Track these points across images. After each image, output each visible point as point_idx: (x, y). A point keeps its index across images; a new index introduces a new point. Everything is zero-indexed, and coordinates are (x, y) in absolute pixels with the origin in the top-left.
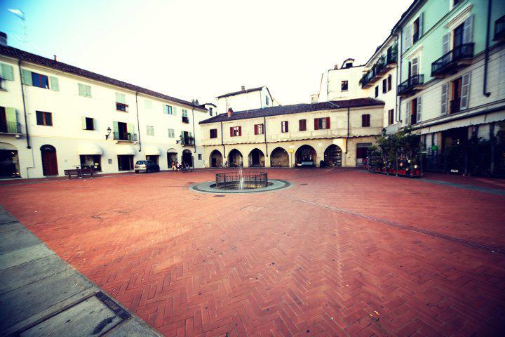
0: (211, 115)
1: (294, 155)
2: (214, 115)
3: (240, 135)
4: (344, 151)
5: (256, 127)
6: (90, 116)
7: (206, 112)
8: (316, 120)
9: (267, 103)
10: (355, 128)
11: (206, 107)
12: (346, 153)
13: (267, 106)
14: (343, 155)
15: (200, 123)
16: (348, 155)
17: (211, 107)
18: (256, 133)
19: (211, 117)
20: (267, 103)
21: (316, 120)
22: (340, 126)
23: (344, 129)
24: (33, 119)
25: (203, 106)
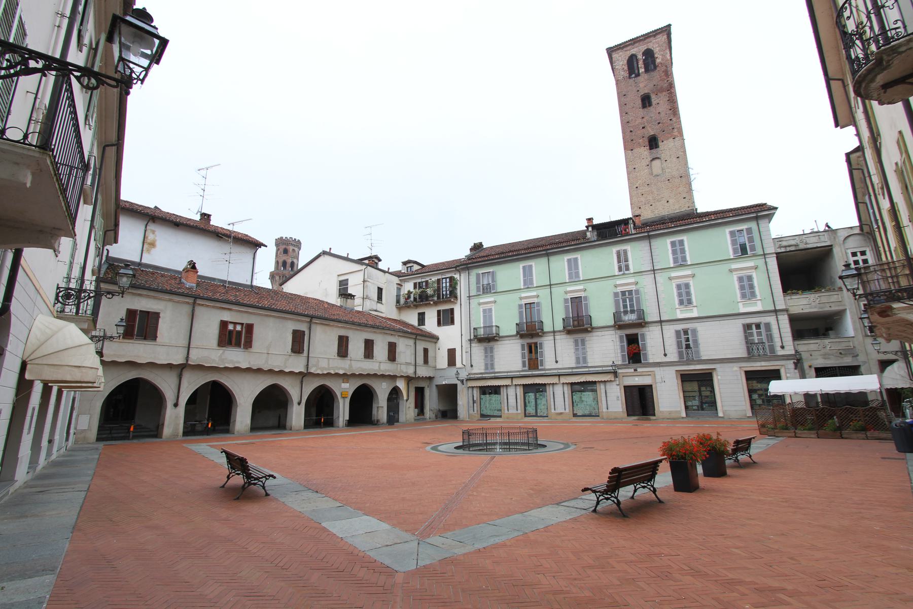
1: (348, 401)
10: (400, 367)
12: (407, 400)
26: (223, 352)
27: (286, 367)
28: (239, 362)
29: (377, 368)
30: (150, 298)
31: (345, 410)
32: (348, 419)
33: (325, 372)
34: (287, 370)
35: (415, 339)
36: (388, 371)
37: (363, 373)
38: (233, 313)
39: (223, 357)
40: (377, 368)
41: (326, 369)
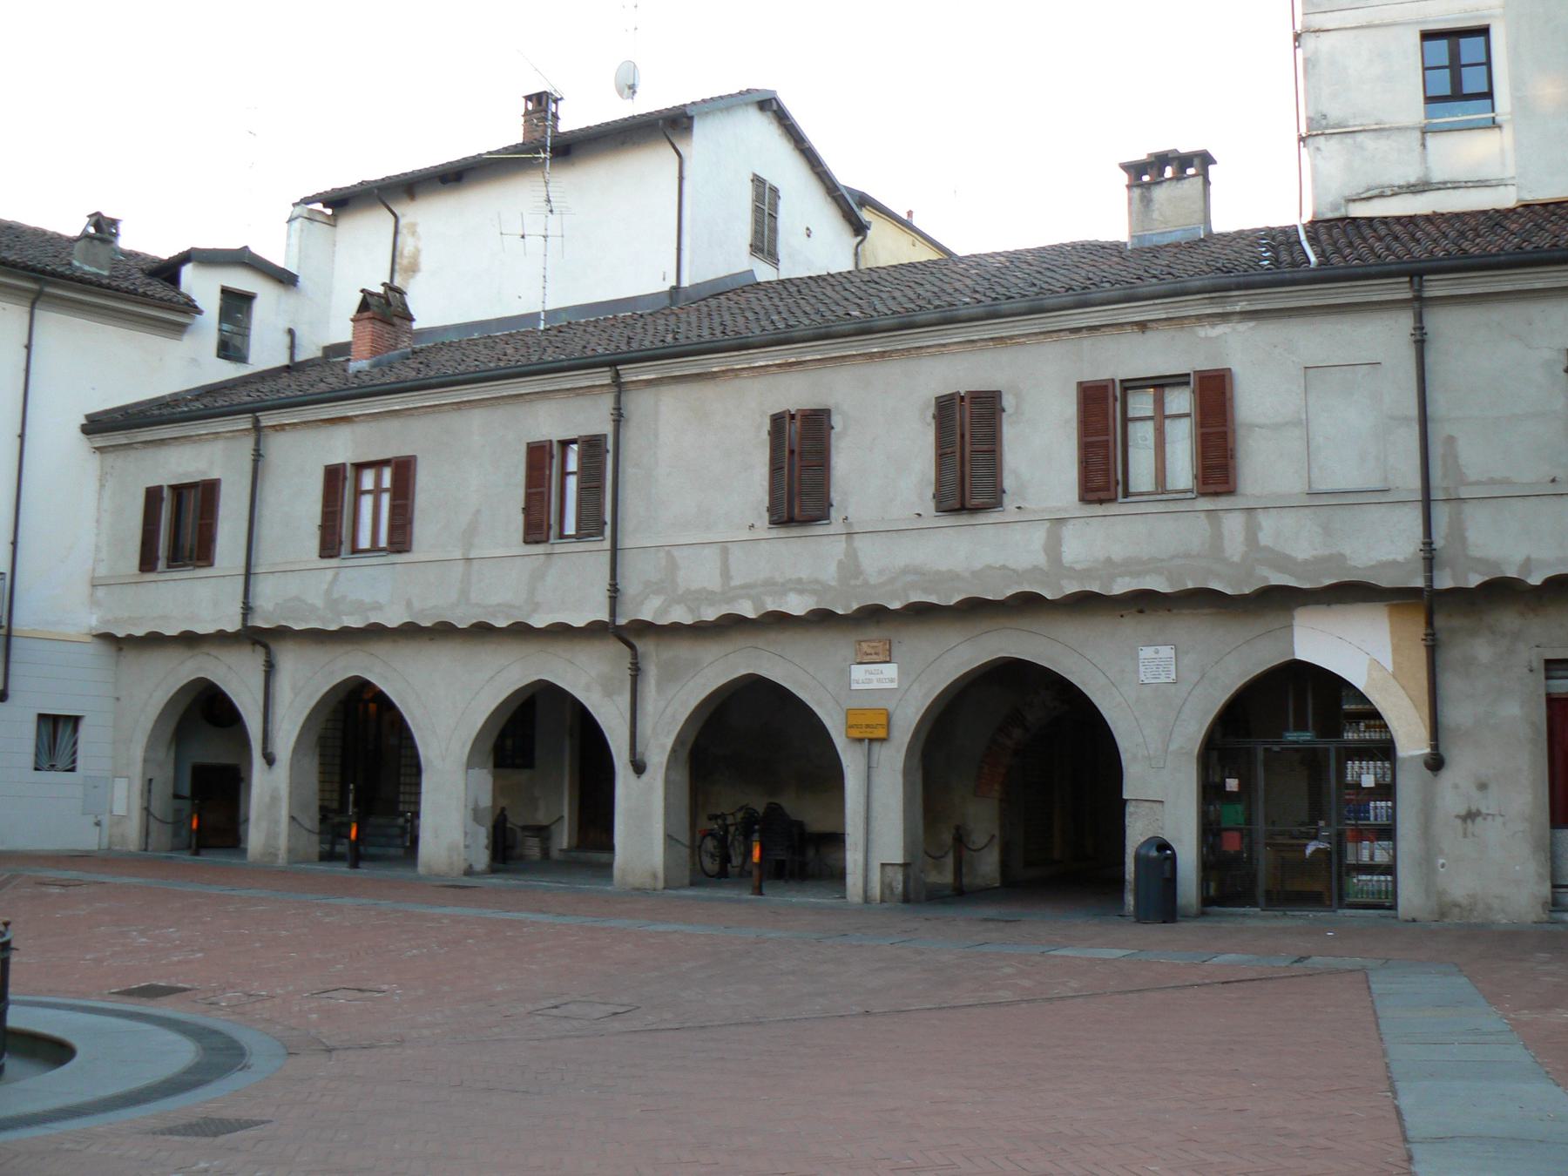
0: (230, 349)
1: (892, 760)
2: (266, 352)
3: (400, 538)
4: (1411, 739)
5: (539, 457)
6: (108, 213)
7: (179, 329)
8: (946, 408)
9: (764, 244)
10: (1503, 494)
11: (201, 286)
12: (1435, 763)
13: (764, 273)
14: (1409, 785)
15: (96, 425)
16: (1453, 791)
17: (241, 280)
18: (537, 528)
19: (229, 371)
20: (764, 244)
21: (946, 408)
22: (1343, 473)
23: (1379, 495)
24: (144, 853)
25: (168, 271)
26: (336, 578)
27: (536, 608)
28: (378, 607)
29: (1041, 560)
30: (168, 444)
31: (877, 807)
32: (898, 857)
33: (710, 615)
34: (539, 622)
35: (1419, 304)
36: (1130, 566)
37: (933, 599)
38: (361, 429)
39: (335, 596)
40: (1041, 560)
41: (708, 597)
